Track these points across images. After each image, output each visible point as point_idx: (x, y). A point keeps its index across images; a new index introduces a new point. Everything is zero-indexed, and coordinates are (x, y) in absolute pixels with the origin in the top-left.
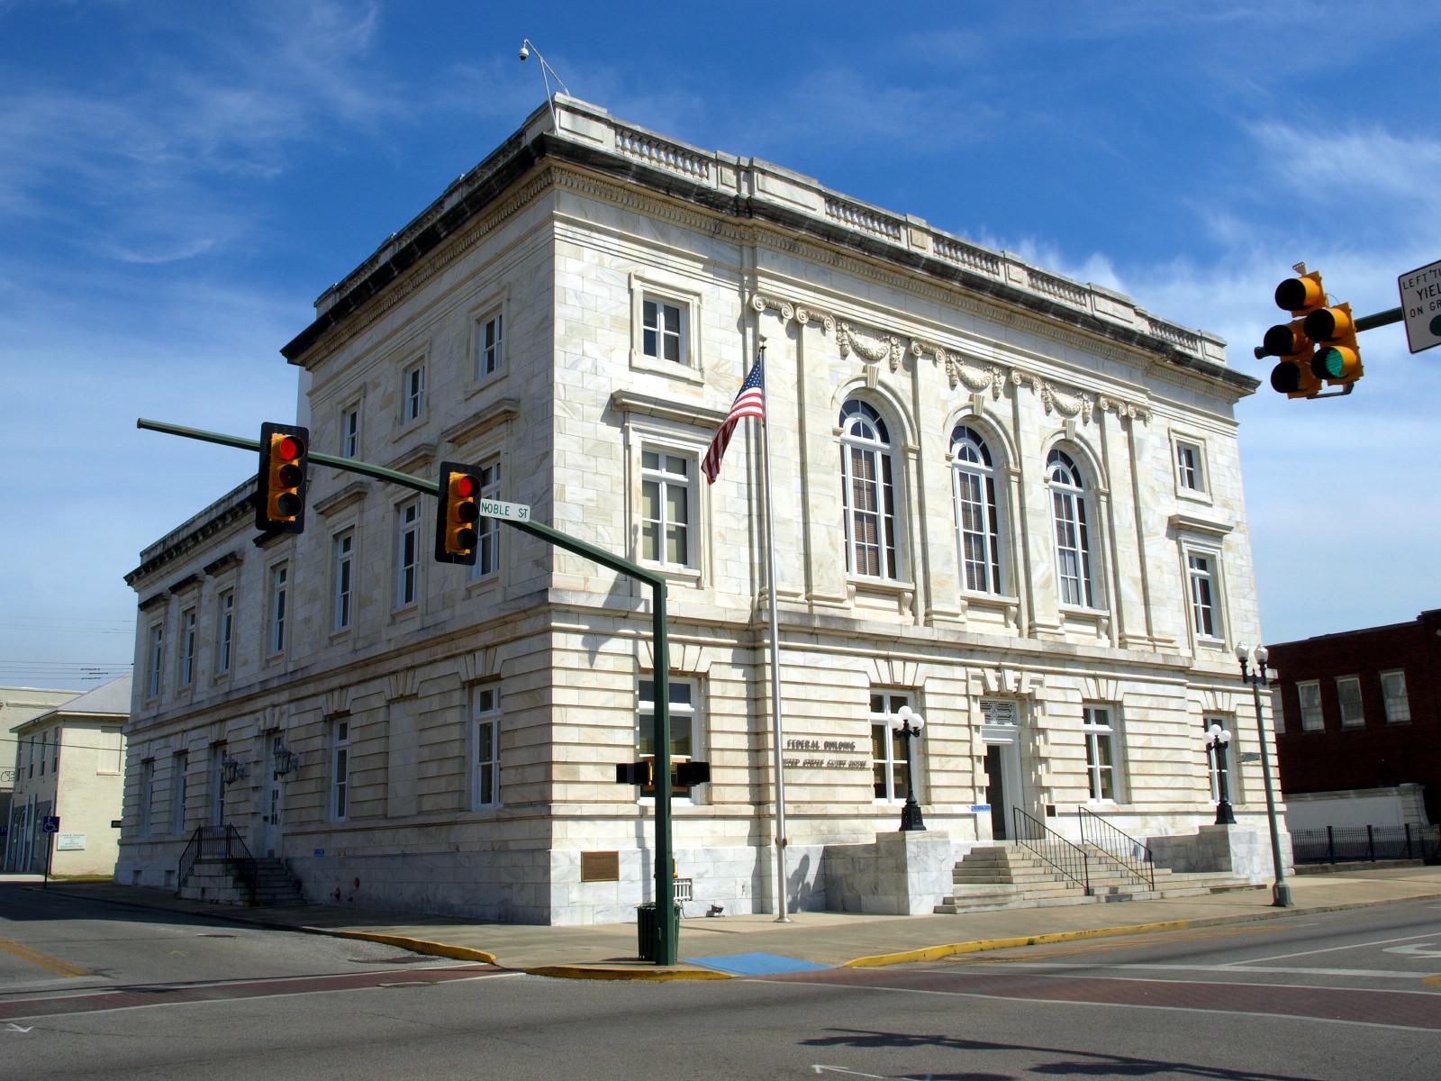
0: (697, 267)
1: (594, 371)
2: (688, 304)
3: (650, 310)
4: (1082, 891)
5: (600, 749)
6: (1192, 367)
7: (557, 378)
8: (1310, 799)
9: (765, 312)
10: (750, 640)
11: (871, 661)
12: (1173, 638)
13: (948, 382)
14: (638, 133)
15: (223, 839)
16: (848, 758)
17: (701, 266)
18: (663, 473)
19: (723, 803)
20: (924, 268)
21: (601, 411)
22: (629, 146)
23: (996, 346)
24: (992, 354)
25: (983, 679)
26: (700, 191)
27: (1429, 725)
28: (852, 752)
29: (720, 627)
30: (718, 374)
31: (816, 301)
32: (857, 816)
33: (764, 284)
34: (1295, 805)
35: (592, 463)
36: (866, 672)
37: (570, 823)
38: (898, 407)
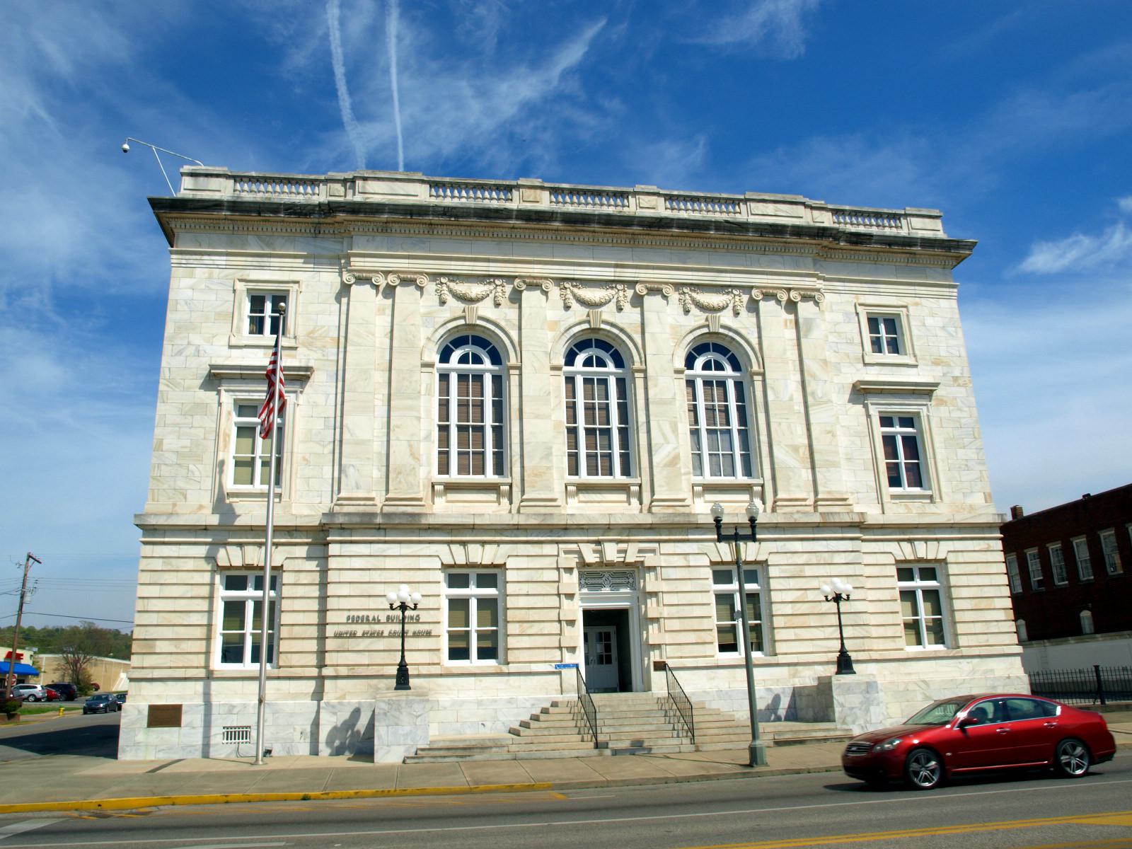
0: (299, 262)
1: (196, 354)
2: (899, 314)
3: (873, 323)
4: (592, 745)
5: (175, 628)
6: (876, 243)
7: (164, 364)
8: (1072, 642)
9: (763, 299)
10: (319, 537)
11: (445, 547)
12: (845, 497)
13: (563, 305)
14: (253, 177)
17: (302, 261)
18: (897, 429)
19: (291, 667)
20: (517, 218)
21: (847, 396)
22: (842, 221)
23: (616, 266)
24: (613, 274)
25: (579, 553)
26: (287, 207)
27: (1096, 564)
29: (296, 530)
30: (312, 338)
31: (410, 266)
33: (357, 263)
34: (1030, 650)
35: (189, 419)
37: (144, 684)
38: (742, 342)
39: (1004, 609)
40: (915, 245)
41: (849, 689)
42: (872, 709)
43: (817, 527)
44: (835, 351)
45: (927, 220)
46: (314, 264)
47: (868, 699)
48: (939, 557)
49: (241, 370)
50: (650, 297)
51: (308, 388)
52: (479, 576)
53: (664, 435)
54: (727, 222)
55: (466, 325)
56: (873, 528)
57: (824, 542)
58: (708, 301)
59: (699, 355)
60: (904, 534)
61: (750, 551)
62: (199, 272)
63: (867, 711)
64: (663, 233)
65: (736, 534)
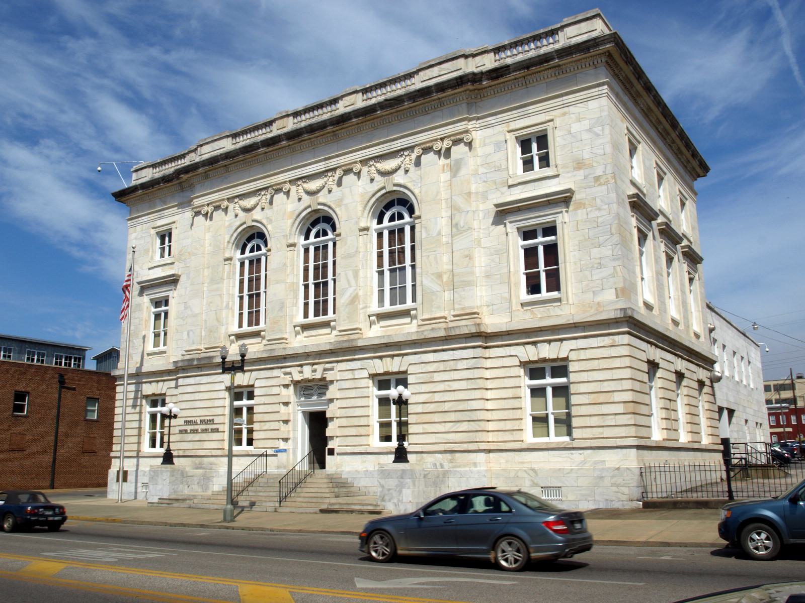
0: (175, 210)
15: (138, 461)
16: (210, 427)
17: (176, 208)
20: (263, 147)
21: (491, 220)
23: (326, 159)
28: (213, 424)
32: (212, 456)
36: (365, 368)
39: (624, 402)
40: (553, 59)
41: (389, 474)
42: (404, 491)
43: (447, 339)
44: (484, 182)
45: (583, 24)
46: (182, 208)
47: (402, 483)
48: (561, 356)
49: (547, 197)
50: (456, 147)
51: (178, 286)
52: (553, 368)
53: (348, 281)
54: (386, 100)
55: (386, 193)
56: (502, 335)
57: (451, 352)
58: (391, 166)
59: (387, 211)
60: (529, 337)
61: (241, 379)
62: (139, 228)
63: (400, 492)
64: (348, 125)
65: (233, 366)
